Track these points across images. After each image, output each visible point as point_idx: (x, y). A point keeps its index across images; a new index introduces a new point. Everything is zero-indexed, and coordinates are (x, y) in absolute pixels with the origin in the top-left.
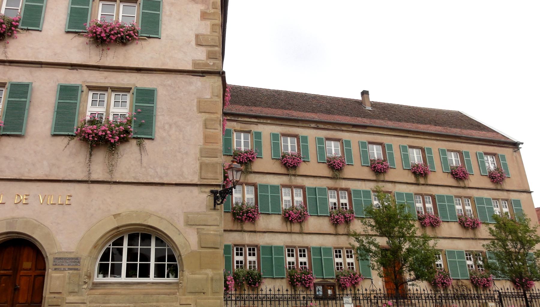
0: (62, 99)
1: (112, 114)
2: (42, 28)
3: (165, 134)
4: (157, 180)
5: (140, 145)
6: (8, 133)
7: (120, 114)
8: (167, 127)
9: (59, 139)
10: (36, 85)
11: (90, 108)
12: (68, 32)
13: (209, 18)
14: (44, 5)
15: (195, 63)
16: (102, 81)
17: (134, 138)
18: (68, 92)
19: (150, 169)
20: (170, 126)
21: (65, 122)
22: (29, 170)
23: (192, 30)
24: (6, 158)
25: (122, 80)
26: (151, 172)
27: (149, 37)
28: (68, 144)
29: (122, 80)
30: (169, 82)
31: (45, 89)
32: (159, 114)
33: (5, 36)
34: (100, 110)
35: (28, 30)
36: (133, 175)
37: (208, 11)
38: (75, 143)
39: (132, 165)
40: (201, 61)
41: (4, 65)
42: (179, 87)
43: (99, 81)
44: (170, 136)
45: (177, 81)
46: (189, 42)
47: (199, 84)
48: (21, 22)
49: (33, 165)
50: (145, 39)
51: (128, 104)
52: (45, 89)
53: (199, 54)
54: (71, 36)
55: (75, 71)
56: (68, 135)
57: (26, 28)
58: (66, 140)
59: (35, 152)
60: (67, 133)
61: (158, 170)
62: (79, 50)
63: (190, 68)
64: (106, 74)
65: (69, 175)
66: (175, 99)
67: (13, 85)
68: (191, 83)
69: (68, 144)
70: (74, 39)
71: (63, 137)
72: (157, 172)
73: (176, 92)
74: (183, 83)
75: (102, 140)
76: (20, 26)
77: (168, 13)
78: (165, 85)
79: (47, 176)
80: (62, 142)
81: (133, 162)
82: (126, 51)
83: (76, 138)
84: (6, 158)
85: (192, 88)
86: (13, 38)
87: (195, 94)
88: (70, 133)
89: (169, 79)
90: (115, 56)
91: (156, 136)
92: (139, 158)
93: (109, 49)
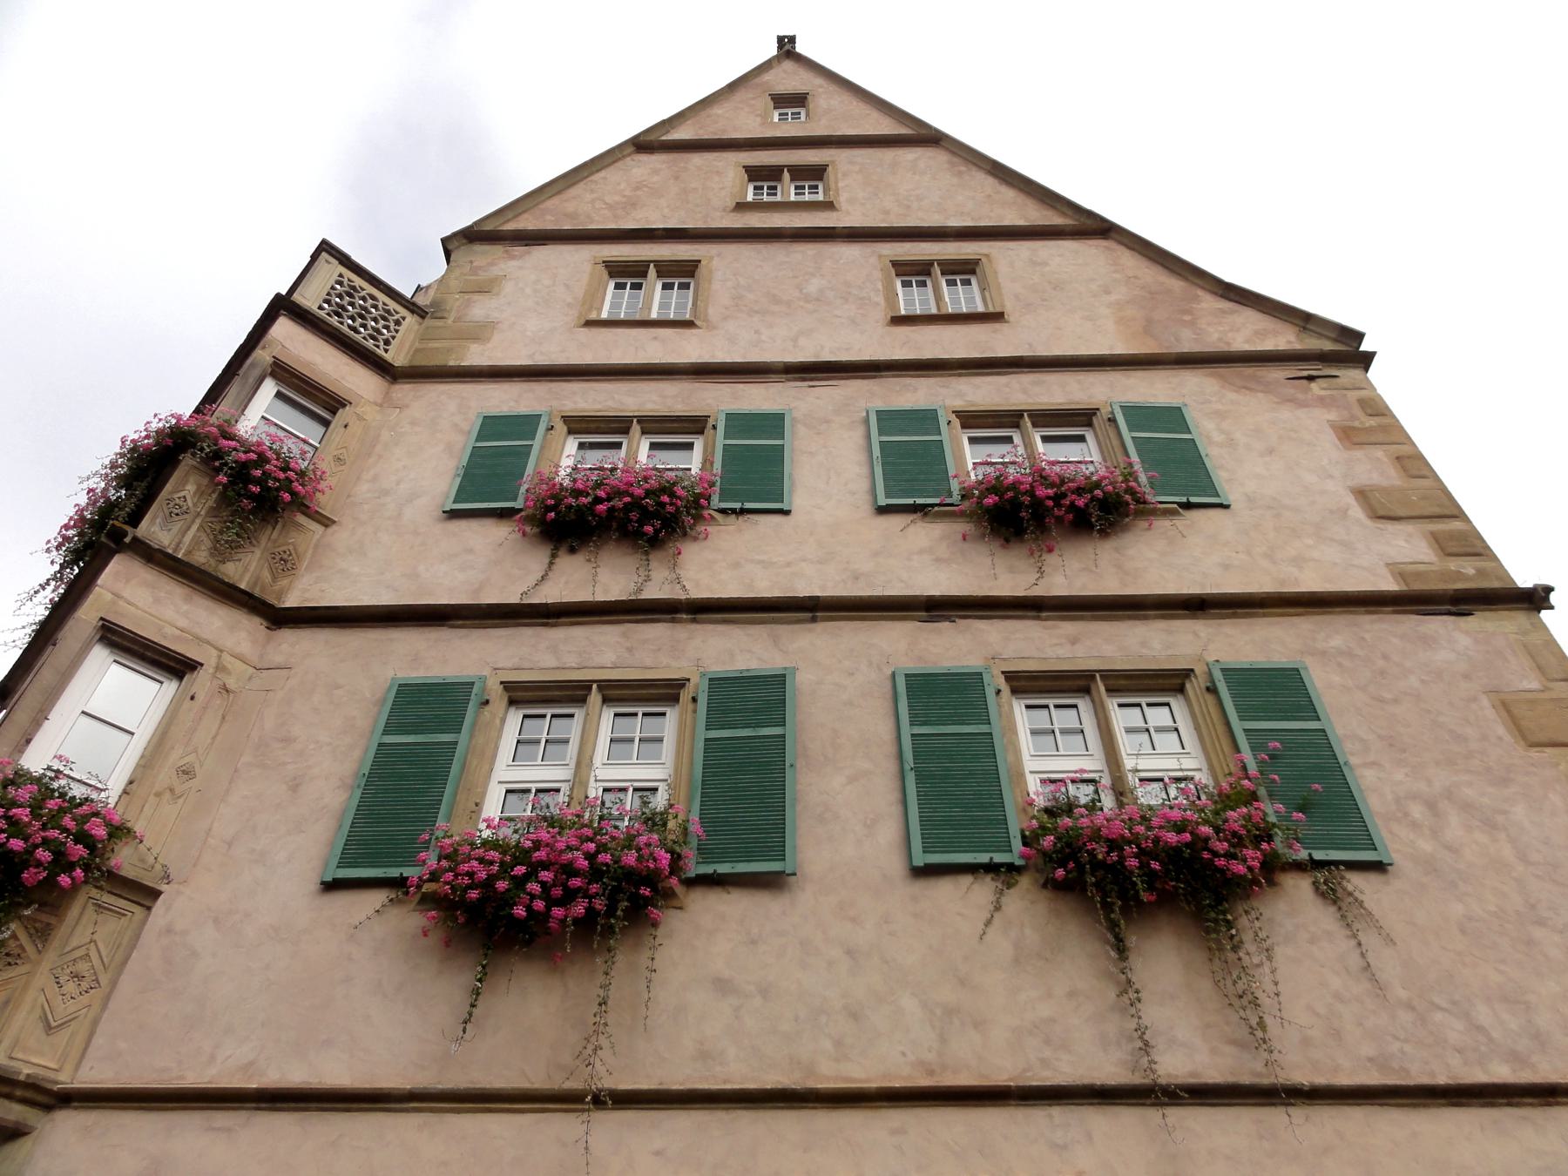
0: (924, 723)
1: (504, 788)
2: (790, 503)
3: (1426, 846)
4: (1501, 1073)
5: (1330, 894)
6: (724, 868)
7: (533, 787)
8: (1417, 811)
9: (945, 890)
10: (803, 680)
11: (1045, 756)
12: (883, 510)
13: (1373, 439)
14: (787, 442)
15: (1400, 573)
16: (1064, 652)
17: (1299, 867)
18: (938, 699)
19: (1438, 1016)
20: (1431, 805)
21: (953, 813)
22: (838, 1043)
23: (1331, 477)
24: (723, 986)
25: (1143, 644)
26: (1455, 1030)
27: (1188, 506)
28: (998, 908)
29: (1143, 644)
30: (1337, 642)
31: (845, 694)
32: (1353, 760)
33: (674, 530)
34: (552, 773)
35: (743, 512)
36: (1368, 1050)
37: (1356, 424)
38: (1025, 905)
39: (1337, 996)
40: (1422, 568)
41: (673, 621)
42: (1385, 657)
43: (1050, 653)
44: (1452, 849)
45: (1367, 636)
46: (1343, 513)
47: (1464, 641)
48: (717, 488)
49: (855, 1016)
50: (1173, 513)
51: (668, 748)
52: (845, 694)
53: (1402, 543)
54: (896, 521)
55: (944, 625)
56: (991, 868)
57: (737, 506)
58: (982, 891)
59: (849, 953)
60: (983, 858)
61: (1483, 1014)
62: (938, 560)
63: (1389, 585)
64: (1068, 628)
65: (1044, 1062)
66: (1396, 701)
67: (719, 684)
68: (1428, 641)
69: (998, 908)
70: (912, 529)
71: (966, 880)
72: (1480, 1029)
73: (1382, 673)
74: (1395, 641)
75: (1150, 883)
76: (715, 501)
77: (1218, 437)
78: (1323, 653)
79: (931, 1073)
80: (964, 901)
81: (1336, 983)
82: (1117, 550)
83: (1025, 881)
84: (723, 986)
85: (1442, 656)
86: (695, 539)
87: (1466, 677)
88: (999, 858)
89: (1336, 632)
90: (1076, 570)
91: (1394, 855)
92: (1354, 960)
93: (1050, 550)
